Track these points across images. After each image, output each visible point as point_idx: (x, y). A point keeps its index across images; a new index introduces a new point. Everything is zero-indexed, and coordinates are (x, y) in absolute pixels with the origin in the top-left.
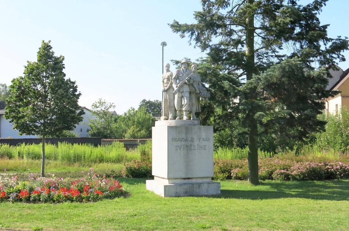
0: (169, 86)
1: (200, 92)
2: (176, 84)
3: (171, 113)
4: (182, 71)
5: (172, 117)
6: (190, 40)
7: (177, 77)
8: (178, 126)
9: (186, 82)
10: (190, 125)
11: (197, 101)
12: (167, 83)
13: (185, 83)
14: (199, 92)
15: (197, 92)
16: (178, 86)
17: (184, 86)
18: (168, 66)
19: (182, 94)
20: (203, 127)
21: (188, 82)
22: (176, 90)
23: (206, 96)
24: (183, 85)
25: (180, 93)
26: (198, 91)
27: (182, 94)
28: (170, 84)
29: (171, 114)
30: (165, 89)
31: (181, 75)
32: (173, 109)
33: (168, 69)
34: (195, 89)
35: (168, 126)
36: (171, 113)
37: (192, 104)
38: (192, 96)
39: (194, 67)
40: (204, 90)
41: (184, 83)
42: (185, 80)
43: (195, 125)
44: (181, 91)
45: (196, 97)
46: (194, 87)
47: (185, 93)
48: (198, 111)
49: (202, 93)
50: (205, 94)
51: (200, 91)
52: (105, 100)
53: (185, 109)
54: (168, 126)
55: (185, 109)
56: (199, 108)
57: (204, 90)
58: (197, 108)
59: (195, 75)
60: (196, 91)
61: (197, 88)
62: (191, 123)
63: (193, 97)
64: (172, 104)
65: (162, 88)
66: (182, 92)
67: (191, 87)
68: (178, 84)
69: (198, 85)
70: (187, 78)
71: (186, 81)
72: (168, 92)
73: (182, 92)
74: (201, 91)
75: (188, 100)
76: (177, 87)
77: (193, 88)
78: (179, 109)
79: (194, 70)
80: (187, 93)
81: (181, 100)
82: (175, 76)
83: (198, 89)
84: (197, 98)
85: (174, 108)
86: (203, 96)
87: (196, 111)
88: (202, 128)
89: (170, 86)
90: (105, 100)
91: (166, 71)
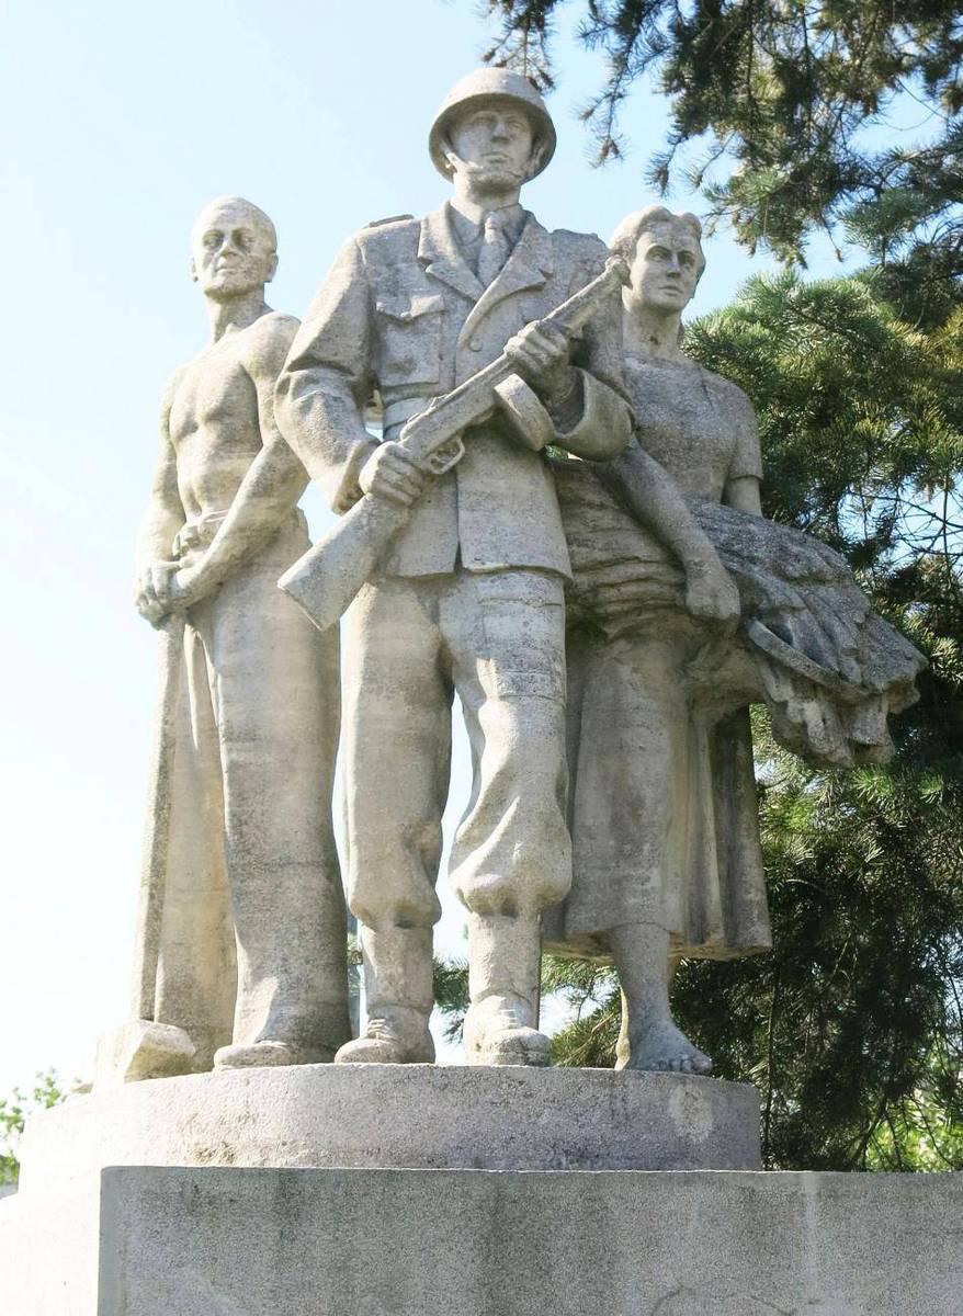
0: (240, 530)
1: (750, 612)
2: (338, 458)
3: (258, 974)
4: (447, 248)
5: (272, 1031)
6: (614, 97)
7: (350, 348)
8: (319, 1177)
9: (499, 410)
10: (582, 1156)
11: (705, 762)
12: (218, 486)
13: (496, 429)
14: (730, 605)
15: (697, 599)
16: (367, 477)
17: (469, 484)
18: (238, 238)
19: (435, 617)
20: (830, 1195)
21: (531, 398)
22: (329, 547)
23: (854, 672)
24: (446, 449)
25: (409, 604)
26: (714, 593)
27: (435, 617)
28: (262, 490)
29: (269, 988)
30: (183, 579)
31: (420, 304)
32: (300, 891)
33: (241, 281)
34: (674, 559)
35: (115, 1180)
36: (258, 974)
37: (626, 809)
38: (625, 672)
39: (644, 245)
40: (819, 563)
41: (470, 433)
42: (500, 375)
43: (679, 1154)
44: (423, 555)
45: (692, 704)
46: (647, 524)
47: (485, 588)
48: (715, 947)
49: (790, 624)
50: (846, 639)
51: (745, 585)
52: (53, 1071)
53: (487, 866)
54: (115, 1180)
55: (489, 879)
56: (731, 879)
57: (818, 579)
58: (699, 866)
59: (660, 363)
60: (682, 587)
61: (699, 545)
62: (596, 1126)
63: (632, 698)
64: (287, 813)
65: (142, 565)
66: (436, 586)
67: (607, 519)
68: (361, 457)
69: (712, 507)
70: (515, 344)
71: (510, 386)
72: (224, 630)
73: (436, 586)
74: (771, 582)
75: (548, 714)
76: (350, 494)
77: (640, 547)
78: (398, 885)
79: (649, 279)
80: (520, 585)
81: (424, 719)
82: (327, 335)
83: (725, 550)
84: (705, 717)
85: (318, 881)
86: (811, 669)
87: (698, 926)
88: (812, 1216)
89: (263, 514)
90: (53, 1071)
91: (214, 310)
